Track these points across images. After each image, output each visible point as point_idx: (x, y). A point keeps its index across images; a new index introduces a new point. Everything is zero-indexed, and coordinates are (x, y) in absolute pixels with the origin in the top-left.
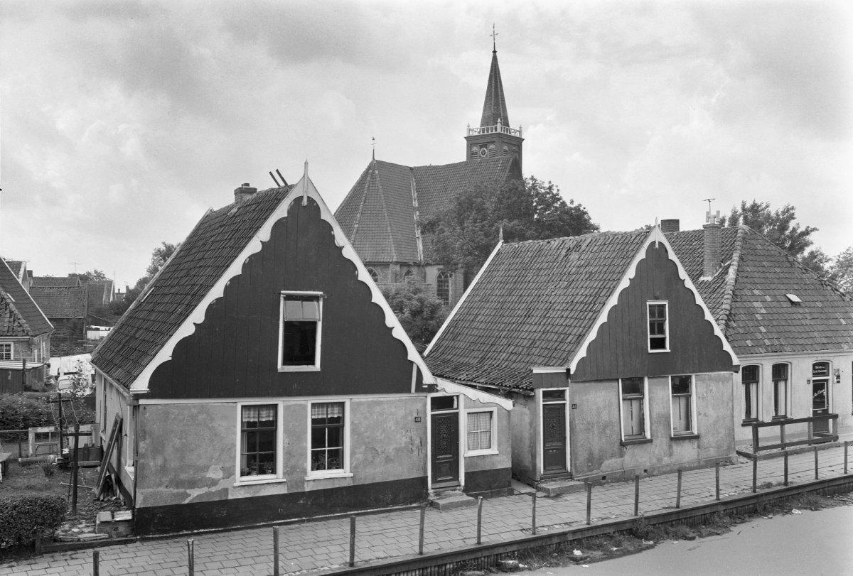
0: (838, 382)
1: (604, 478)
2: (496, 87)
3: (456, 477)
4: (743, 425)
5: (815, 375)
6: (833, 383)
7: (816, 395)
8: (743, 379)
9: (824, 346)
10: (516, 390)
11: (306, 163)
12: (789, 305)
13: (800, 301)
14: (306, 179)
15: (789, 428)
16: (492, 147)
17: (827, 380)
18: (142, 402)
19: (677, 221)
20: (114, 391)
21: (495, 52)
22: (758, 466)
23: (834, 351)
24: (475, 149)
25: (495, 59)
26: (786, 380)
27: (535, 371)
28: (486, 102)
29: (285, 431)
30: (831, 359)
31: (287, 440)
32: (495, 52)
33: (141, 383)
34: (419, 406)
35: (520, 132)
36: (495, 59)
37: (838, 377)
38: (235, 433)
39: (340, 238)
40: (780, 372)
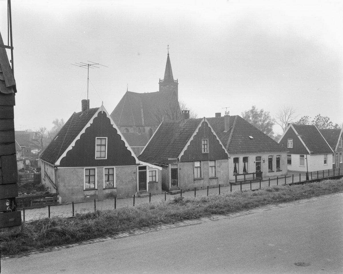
0: (264, 162)
1: (189, 189)
2: (169, 66)
3: (146, 189)
4: (269, 172)
5: (256, 160)
6: (262, 162)
7: (257, 166)
8: (234, 162)
9: (260, 151)
10: (164, 165)
11: (103, 102)
12: (249, 139)
13: (253, 138)
14: (102, 106)
15: (247, 176)
16: (168, 86)
17: (261, 162)
18: (58, 168)
19: (220, 113)
20: (48, 165)
21: (168, 54)
22: (242, 186)
23: (259, 153)
24: (162, 87)
25: (168, 57)
26: (247, 162)
27: (168, 159)
28: (165, 71)
29: (97, 176)
30: (262, 155)
31: (98, 178)
32: (168, 54)
33: (58, 163)
34: (135, 169)
35: (177, 81)
36: (168, 57)
37: (264, 161)
38: (84, 176)
39: (112, 122)
40: (245, 160)
